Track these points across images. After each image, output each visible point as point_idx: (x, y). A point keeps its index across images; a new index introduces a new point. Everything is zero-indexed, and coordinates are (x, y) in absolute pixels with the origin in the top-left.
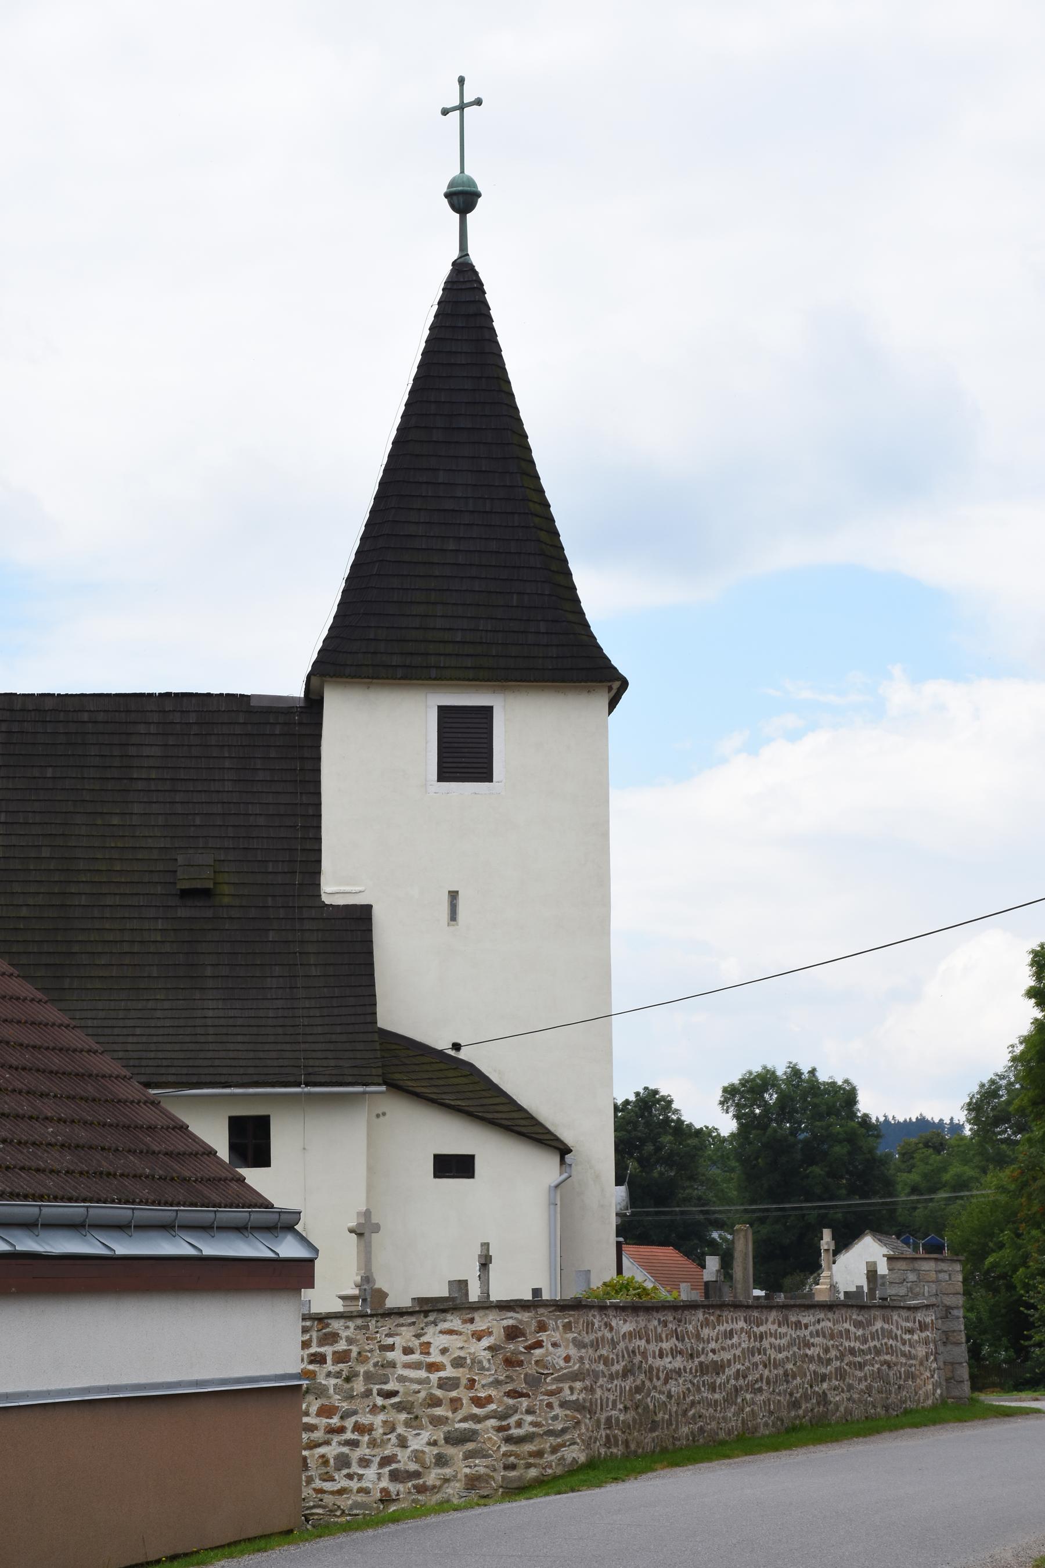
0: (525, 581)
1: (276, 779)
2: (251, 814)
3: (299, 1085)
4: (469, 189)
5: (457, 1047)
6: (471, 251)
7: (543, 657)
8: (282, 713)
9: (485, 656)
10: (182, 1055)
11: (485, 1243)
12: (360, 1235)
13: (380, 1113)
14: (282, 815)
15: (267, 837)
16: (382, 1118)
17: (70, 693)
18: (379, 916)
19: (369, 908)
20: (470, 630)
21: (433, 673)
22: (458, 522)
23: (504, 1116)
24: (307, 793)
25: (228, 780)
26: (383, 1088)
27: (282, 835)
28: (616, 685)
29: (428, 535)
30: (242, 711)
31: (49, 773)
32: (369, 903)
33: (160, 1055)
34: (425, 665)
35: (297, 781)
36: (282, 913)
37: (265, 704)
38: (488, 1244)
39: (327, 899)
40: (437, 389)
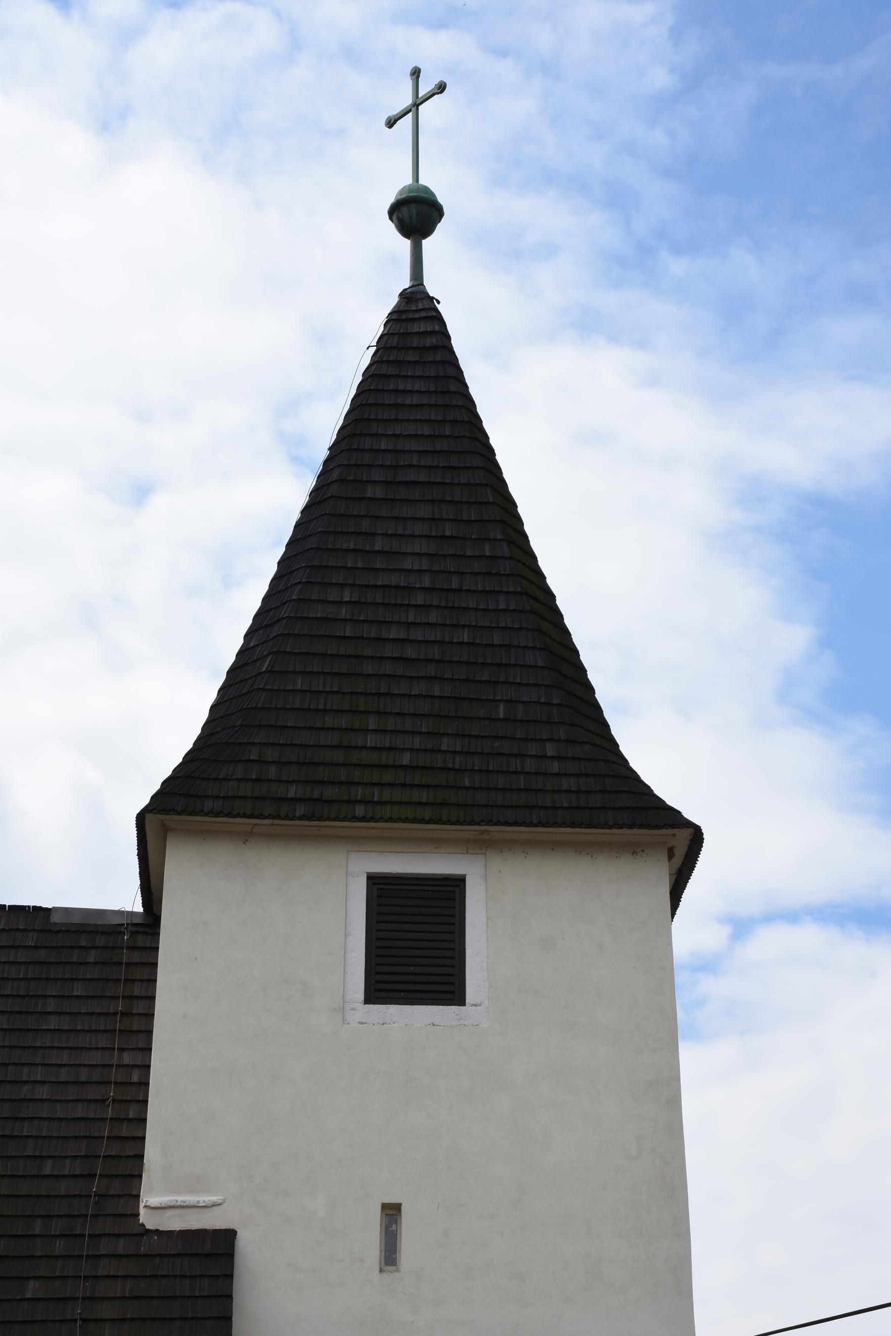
0: (519, 684)
1: (79, 1028)
2: (25, 1082)
4: (426, 196)
7: (553, 791)
8: (103, 933)
9: (452, 787)
14: (83, 1083)
15: (50, 1119)
18: (245, 1244)
19: (229, 1236)
20: (426, 750)
21: (360, 810)
22: (407, 602)
24: (132, 1049)
27: (79, 1115)
29: (356, 618)
30: (34, 930)
32: (231, 1227)
34: (346, 798)
35: (115, 1030)
36: (59, 1247)
37: (76, 920)
39: (147, 1219)
40: (373, 435)
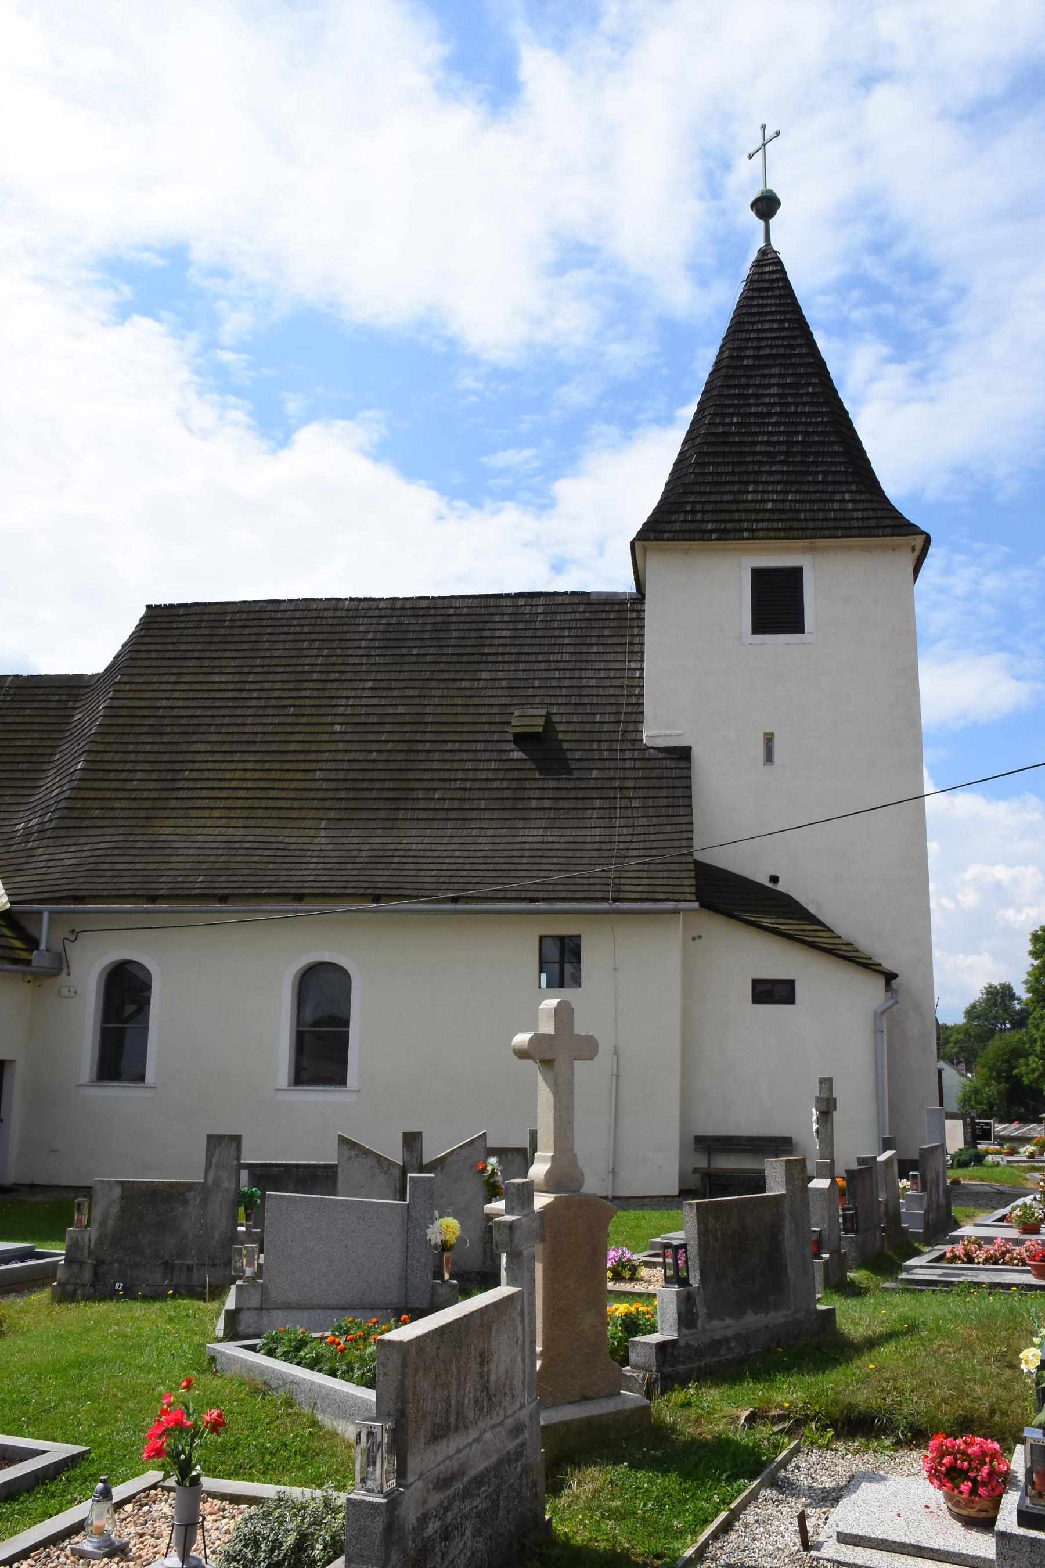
3: (605, 900)
5: (774, 879)
6: (772, 243)
10: (494, 874)
11: (826, 1080)
12: (547, 1063)
13: (696, 935)
16: (697, 940)
17: (441, 595)
18: (696, 754)
23: (825, 940)
25: (566, 653)
26: (696, 905)
28: (919, 541)
31: (415, 651)
32: (756, 1006)
33: (473, 874)
36: (606, 755)
38: (829, 1081)
